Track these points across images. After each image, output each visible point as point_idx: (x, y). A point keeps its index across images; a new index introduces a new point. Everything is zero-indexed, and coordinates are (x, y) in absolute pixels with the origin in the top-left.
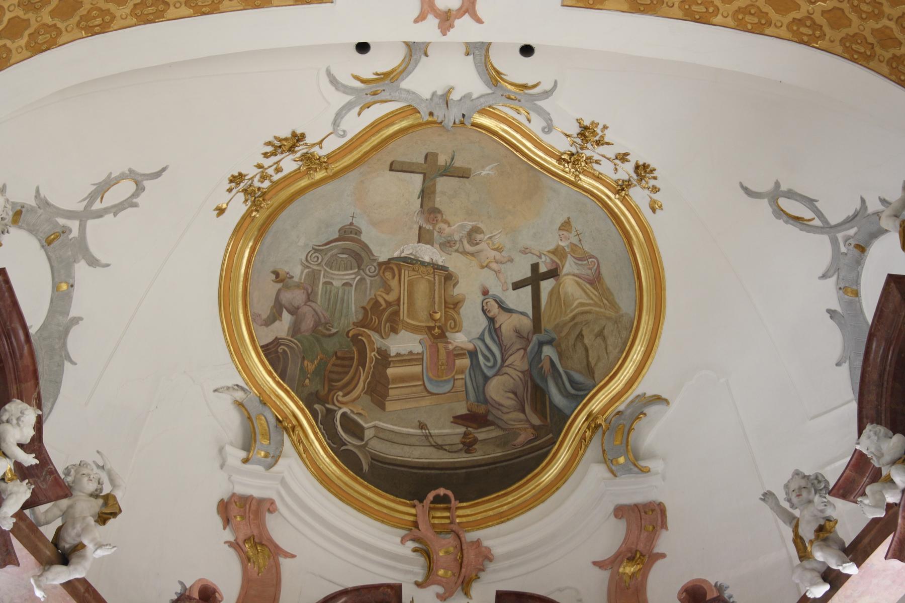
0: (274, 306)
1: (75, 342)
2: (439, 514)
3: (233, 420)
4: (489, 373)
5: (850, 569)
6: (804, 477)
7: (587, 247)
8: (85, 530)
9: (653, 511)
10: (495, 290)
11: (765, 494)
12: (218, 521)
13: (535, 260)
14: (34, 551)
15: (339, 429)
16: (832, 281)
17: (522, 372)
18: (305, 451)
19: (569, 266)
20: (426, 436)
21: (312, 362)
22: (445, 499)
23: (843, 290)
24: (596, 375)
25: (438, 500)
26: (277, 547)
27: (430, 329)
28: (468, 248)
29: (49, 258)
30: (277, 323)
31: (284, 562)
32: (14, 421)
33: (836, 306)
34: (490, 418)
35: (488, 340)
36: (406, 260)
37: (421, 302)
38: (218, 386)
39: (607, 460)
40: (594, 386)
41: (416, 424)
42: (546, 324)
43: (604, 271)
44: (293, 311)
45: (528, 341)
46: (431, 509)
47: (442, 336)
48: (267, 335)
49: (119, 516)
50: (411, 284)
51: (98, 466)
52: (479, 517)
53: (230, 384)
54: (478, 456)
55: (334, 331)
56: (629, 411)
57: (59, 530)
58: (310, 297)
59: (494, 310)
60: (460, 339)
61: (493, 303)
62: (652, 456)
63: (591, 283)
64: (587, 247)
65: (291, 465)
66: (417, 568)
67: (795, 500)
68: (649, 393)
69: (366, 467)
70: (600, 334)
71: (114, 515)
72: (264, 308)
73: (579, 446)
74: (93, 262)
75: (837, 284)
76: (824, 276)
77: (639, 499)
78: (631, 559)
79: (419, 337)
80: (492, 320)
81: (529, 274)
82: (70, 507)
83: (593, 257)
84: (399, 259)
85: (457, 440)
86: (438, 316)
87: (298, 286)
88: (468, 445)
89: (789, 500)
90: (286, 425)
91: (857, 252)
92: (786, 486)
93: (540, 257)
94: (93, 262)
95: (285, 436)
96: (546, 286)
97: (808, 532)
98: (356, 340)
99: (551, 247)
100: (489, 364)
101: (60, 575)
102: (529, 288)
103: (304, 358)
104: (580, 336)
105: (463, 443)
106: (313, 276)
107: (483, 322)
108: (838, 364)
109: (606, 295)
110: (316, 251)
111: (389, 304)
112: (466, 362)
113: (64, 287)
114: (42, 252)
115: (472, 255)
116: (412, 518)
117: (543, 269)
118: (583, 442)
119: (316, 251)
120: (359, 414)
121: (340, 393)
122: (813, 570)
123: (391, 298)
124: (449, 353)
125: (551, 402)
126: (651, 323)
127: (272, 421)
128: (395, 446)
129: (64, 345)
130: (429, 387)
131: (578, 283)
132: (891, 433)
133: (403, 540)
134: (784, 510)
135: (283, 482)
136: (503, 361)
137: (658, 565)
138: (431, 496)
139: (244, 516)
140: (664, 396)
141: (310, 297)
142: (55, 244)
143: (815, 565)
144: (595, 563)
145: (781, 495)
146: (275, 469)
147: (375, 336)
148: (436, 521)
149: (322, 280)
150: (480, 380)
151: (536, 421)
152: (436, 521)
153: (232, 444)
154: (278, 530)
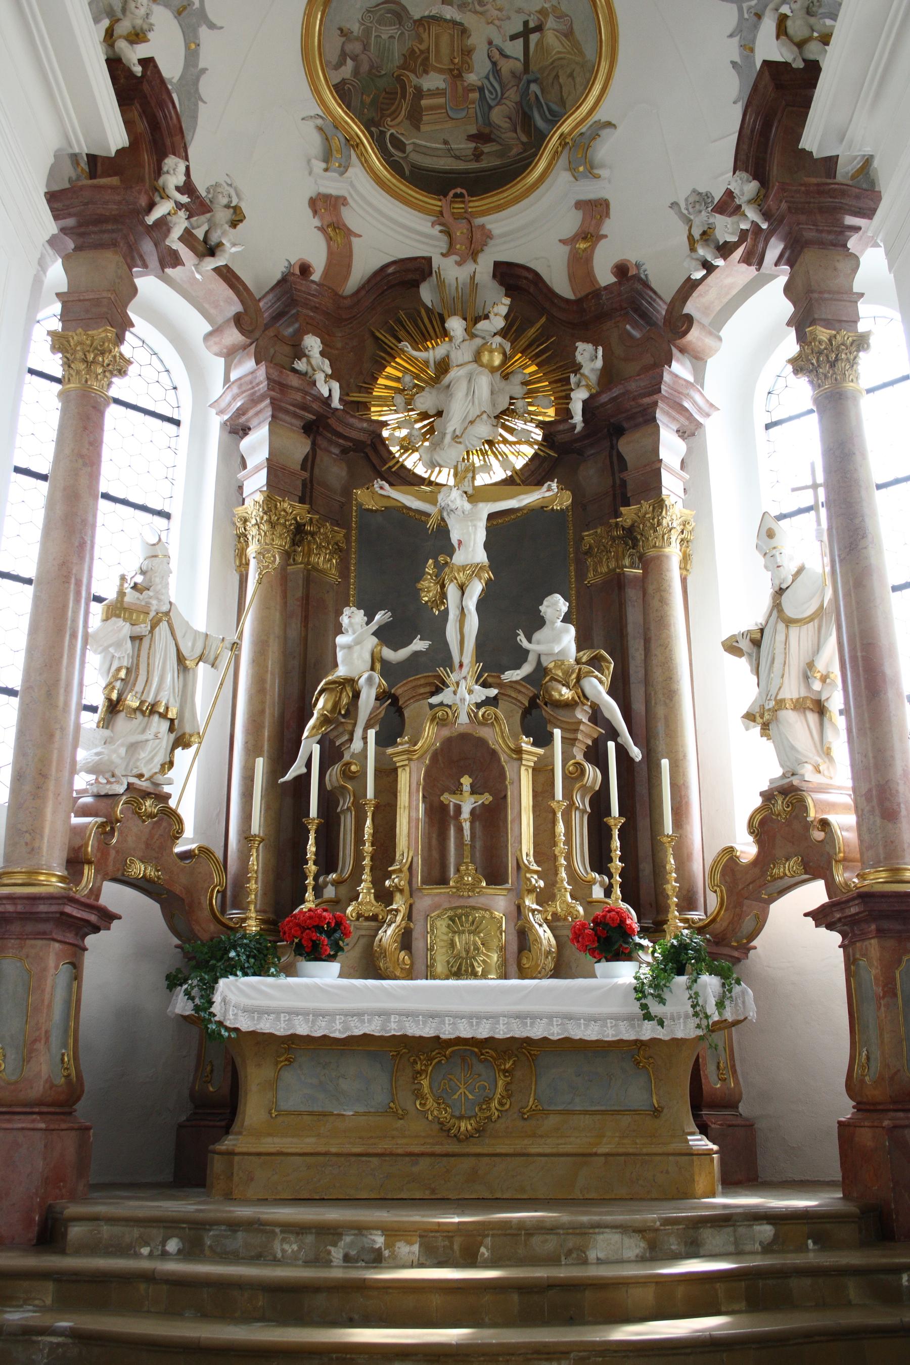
0: (340, 55)
1: (205, 87)
2: (457, 206)
3: (316, 139)
4: (492, 103)
5: (720, 262)
6: (699, 194)
7: (564, 7)
8: (224, 233)
9: (601, 205)
10: (497, 41)
11: (672, 204)
12: (309, 212)
13: (526, 18)
14: (193, 249)
15: (389, 145)
16: (736, 40)
17: (516, 103)
18: (366, 161)
19: (551, 23)
20: (449, 150)
21: (369, 96)
22: (461, 195)
23: (743, 46)
24: (567, 106)
25: (456, 196)
26: (349, 229)
27: (451, 70)
28: (478, 8)
29: (181, 26)
30: (343, 68)
31: (354, 240)
32: (172, 172)
33: (737, 59)
34: (493, 136)
35: (492, 79)
36: (433, 18)
37: (445, 50)
38: (305, 116)
39: (572, 169)
40: (565, 114)
41: (441, 141)
42: (533, 67)
43: (575, 27)
44: (354, 58)
45: (520, 79)
46: (451, 202)
47: (460, 76)
48: (336, 77)
49: (244, 222)
50: (437, 37)
51: (228, 184)
52: (484, 207)
53: (312, 114)
54: (484, 164)
55: (383, 72)
56: (589, 132)
57: (207, 233)
58: (366, 47)
59: (496, 55)
60: (472, 78)
61: (496, 51)
62: (602, 166)
63: (566, 36)
64: (563, 8)
65: (356, 172)
66: (443, 245)
67: (691, 210)
68: (603, 120)
69: (407, 172)
70: (571, 75)
71: (241, 221)
72: (334, 57)
73: (553, 158)
74: (212, 26)
75: (740, 42)
76: (731, 36)
77: (592, 196)
78: (585, 239)
79: (443, 77)
80: (494, 64)
81: (521, 29)
82: (212, 216)
83: (567, 16)
84: (429, 17)
85: (470, 152)
86: (456, 61)
87: (357, 39)
88: (477, 156)
89: (687, 209)
90: (352, 143)
91: (755, 19)
92: (686, 200)
93: (529, 16)
94: (212, 26)
95: (352, 151)
96: (534, 38)
97: (697, 234)
98: (399, 79)
99: (538, 8)
100: (493, 97)
101: (210, 264)
102: (521, 40)
103: (362, 94)
104: (557, 76)
105: (474, 155)
106: (367, 32)
107: (488, 65)
108: (735, 103)
109: (577, 47)
110: (369, 12)
111: (422, 52)
112: (475, 95)
113: (193, 46)
114: (176, 22)
115: (481, 13)
116: (438, 209)
117: (532, 25)
118: (556, 154)
119: (369, 12)
120: (402, 134)
121: (389, 119)
122: (697, 259)
123: (423, 47)
124: (464, 88)
125: (535, 125)
126: (607, 67)
127: (343, 140)
128: (428, 157)
129: (197, 90)
130: (449, 112)
131: (556, 36)
132: (751, 178)
133: (433, 225)
134: (684, 215)
135: (352, 185)
136: (502, 94)
137: (603, 242)
138: (451, 194)
139: (327, 207)
140: (613, 122)
141: (366, 47)
142: (184, 14)
143: (698, 257)
144: (560, 241)
145: (683, 205)
146: (347, 175)
147: (412, 76)
148: (455, 211)
149: (374, 34)
150: (486, 109)
151: (524, 139)
152: (455, 211)
153: (316, 158)
154: (351, 218)
